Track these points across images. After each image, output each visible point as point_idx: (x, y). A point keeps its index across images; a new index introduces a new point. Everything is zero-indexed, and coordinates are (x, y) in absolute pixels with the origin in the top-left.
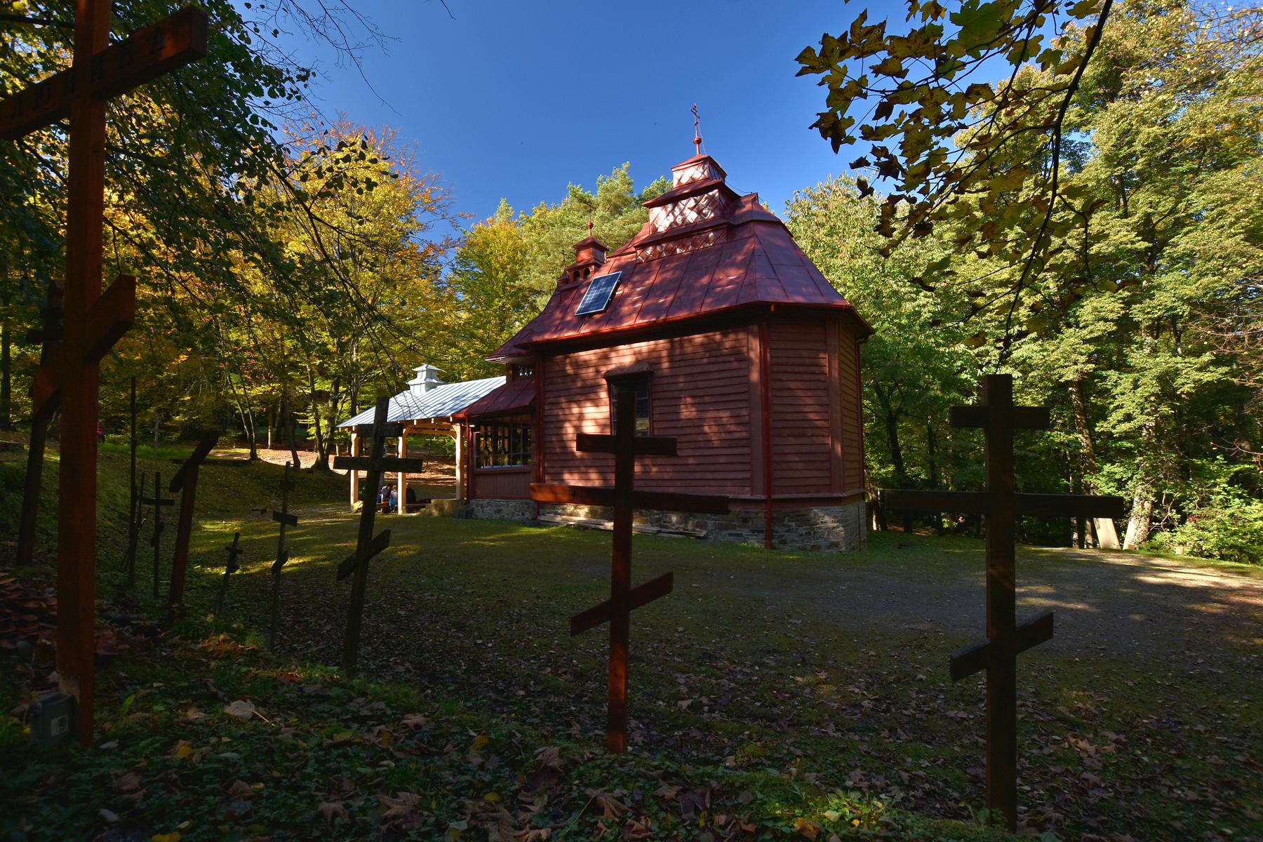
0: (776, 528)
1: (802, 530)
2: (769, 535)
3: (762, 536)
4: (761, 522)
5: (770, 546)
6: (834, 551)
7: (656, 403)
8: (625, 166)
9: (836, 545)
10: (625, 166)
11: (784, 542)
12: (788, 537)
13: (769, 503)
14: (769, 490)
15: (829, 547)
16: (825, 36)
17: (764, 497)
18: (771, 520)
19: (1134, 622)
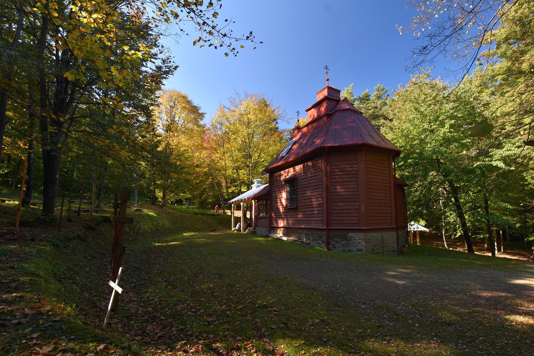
0: (331, 241)
1: (343, 243)
2: (328, 244)
3: (325, 244)
4: (324, 239)
5: (329, 249)
6: (360, 253)
7: (299, 190)
8: (351, 86)
9: (361, 250)
10: (351, 86)
11: (335, 247)
12: (337, 245)
13: (328, 230)
14: (327, 226)
15: (357, 251)
16: (332, 97)
17: (325, 228)
18: (328, 238)
19: (53, 58)
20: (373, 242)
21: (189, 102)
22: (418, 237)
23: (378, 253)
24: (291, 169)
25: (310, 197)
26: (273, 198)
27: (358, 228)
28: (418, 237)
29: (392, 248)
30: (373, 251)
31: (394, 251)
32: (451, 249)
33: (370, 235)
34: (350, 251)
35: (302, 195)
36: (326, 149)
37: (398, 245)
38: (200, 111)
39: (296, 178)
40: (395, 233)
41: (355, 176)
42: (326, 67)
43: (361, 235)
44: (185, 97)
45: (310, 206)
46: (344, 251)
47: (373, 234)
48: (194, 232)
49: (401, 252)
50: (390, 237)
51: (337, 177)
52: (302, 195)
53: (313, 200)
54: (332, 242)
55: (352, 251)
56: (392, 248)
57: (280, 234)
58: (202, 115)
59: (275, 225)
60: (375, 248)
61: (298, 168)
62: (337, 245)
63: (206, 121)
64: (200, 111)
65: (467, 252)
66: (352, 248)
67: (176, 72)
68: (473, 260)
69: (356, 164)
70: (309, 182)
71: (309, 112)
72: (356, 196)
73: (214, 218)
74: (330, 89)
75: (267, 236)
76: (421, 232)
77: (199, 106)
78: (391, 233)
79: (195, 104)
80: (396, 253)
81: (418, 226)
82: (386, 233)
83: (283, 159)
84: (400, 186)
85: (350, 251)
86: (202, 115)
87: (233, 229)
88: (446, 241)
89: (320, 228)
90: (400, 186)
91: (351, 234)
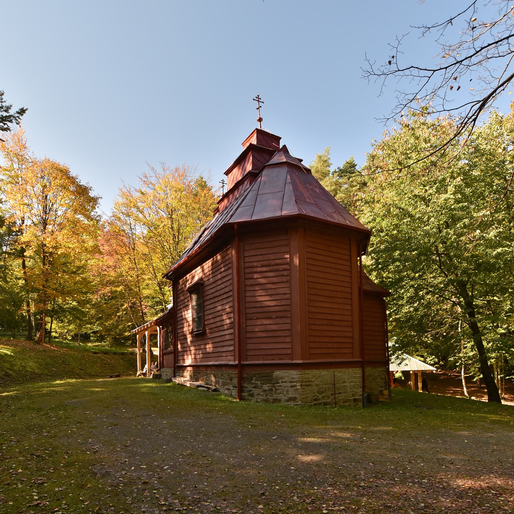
0: (246, 385)
1: (266, 387)
2: (241, 389)
4: (235, 381)
5: (241, 398)
9: (294, 399)
12: (255, 391)
13: (240, 367)
14: (240, 361)
15: (288, 401)
17: (237, 362)
18: (241, 379)
20: (317, 385)
21: (73, 180)
22: (420, 380)
23: (325, 404)
24: (199, 269)
25: (219, 314)
26: (179, 319)
27: (290, 362)
28: (420, 380)
29: (353, 395)
30: (316, 400)
31: (355, 400)
32: (473, 398)
33: (312, 374)
34: (276, 400)
35: (212, 311)
36: (236, 227)
37: (364, 391)
38: (92, 194)
39: (203, 284)
40: (357, 372)
41: (286, 273)
42: (258, 99)
43: (294, 374)
44: (65, 173)
45: (220, 328)
46: (266, 401)
47: (316, 372)
48: (76, 378)
49: (369, 400)
50: (350, 378)
51: (256, 276)
52: (212, 311)
53: (225, 317)
54: (248, 386)
55: (279, 401)
56: (353, 395)
57: (185, 379)
58: (94, 201)
59: (181, 364)
60: (320, 396)
61: (207, 265)
62: (255, 391)
63: (105, 210)
64: (92, 194)
65: (487, 401)
66: (280, 396)
67: (24, 118)
68: (486, 413)
69: (287, 253)
70: (218, 288)
71: (230, 175)
72: (288, 308)
73: (123, 359)
74: (260, 133)
75: (170, 381)
76: (424, 373)
77: (90, 185)
78: (350, 370)
79: (83, 183)
80: (360, 404)
81: (410, 364)
82: (343, 370)
83: (265, 288)
84: (376, 298)
85: (276, 400)
86: (94, 201)
87: (138, 373)
88: (467, 388)
89: (231, 363)
90: (376, 298)
91: (278, 373)
